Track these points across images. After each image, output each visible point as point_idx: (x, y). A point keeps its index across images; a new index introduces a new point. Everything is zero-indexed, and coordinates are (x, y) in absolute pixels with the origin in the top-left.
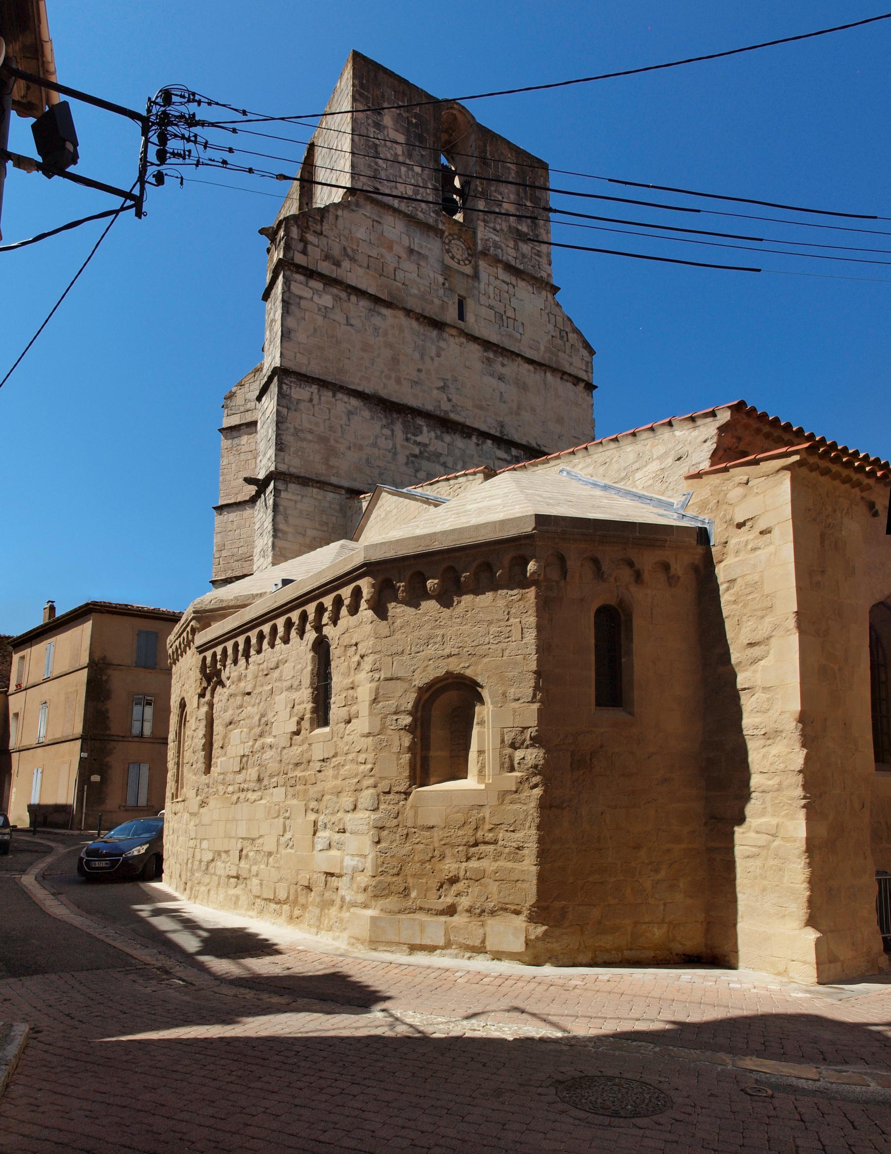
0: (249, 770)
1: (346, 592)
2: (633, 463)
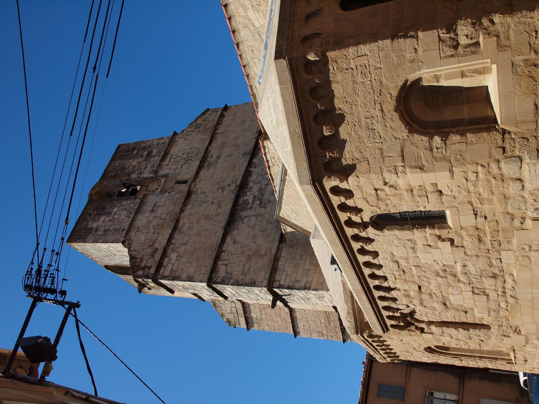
0: (486, 286)
1: (336, 200)
2: (250, 30)
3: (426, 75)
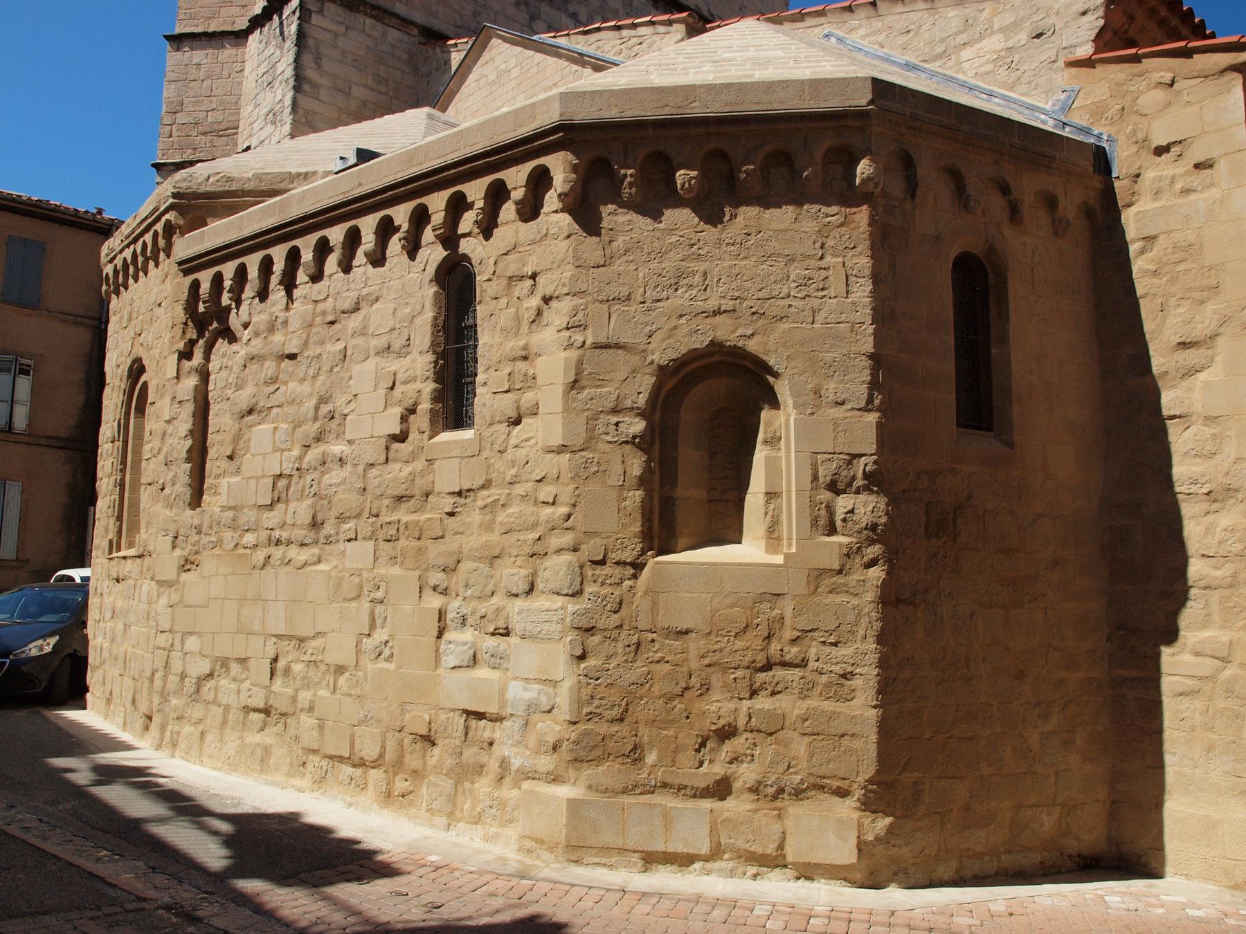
0: (292, 505)
1: (516, 177)
2: (956, 34)
3: (782, 419)
